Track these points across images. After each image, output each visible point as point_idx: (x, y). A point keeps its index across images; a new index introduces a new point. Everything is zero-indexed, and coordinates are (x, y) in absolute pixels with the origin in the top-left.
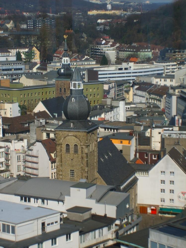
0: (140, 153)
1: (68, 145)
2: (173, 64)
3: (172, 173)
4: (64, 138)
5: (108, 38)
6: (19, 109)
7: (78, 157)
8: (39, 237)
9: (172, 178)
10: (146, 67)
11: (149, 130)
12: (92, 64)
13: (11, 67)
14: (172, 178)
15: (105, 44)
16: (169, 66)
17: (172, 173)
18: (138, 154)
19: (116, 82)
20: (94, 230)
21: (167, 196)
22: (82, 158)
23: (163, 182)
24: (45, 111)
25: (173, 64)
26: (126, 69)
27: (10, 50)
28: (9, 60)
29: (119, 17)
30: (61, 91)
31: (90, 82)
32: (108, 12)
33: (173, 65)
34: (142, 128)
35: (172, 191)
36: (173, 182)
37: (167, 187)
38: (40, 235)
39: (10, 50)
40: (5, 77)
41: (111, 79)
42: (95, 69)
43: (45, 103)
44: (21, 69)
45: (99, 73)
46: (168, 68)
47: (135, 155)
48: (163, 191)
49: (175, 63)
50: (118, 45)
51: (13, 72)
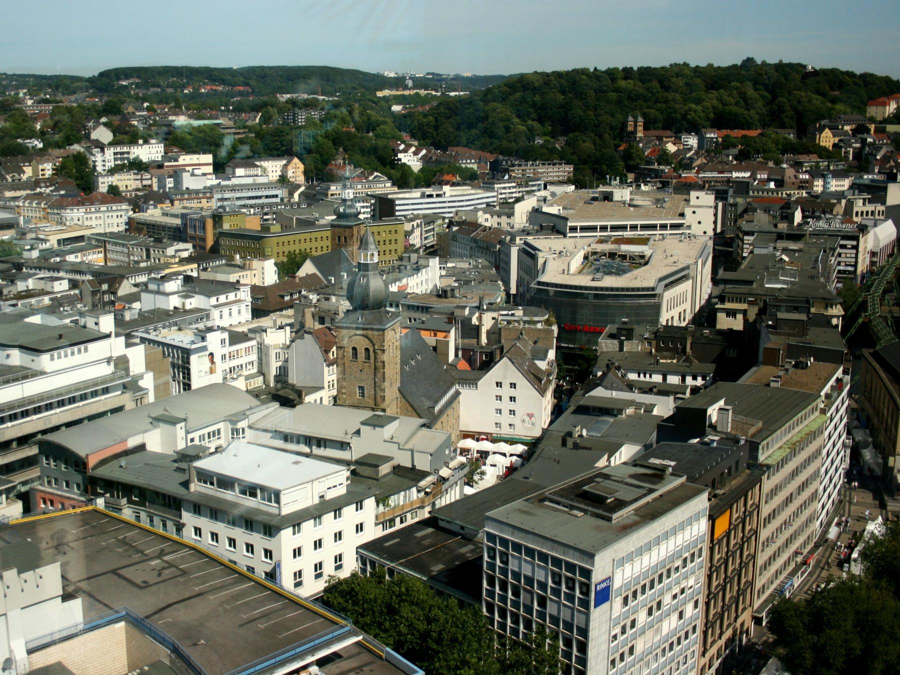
0: (463, 350)
1: (354, 349)
2: (510, 185)
3: (513, 385)
4: (350, 337)
5: (408, 138)
6: (276, 269)
7: (370, 367)
8: (315, 507)
9: (513, 392)
10: (469, 192)
11: (477, 315)
12: (385, 187)
13: (259, 194)
14: (513, 392)
15: (405, 151)
16: (505, 188)
17: (513, 385)
18: (460, 353)
19: (425, 216)
20: (398, 492)
21: (506, 419)
22: (376, 368)
23: (499, 398)
24: (314, 274)
25: (510, 185)
26: (438, 196)
27: (258, 163)
28: (257, 182)
29: (427, 99)
30: (339, 241)
31: (384, 221)
32: (407, 93)
33: (509, 188)
34: (467, 312)
35: (512, 412)
36: (515, 384)
37: (506, 405)
38: (316, 505)
39: (258, 163)
40: (252, 210)
41: (415, 212)
42: (390, 196)
43: (317, 261)
44: (277, 196)
45: (397, 202)
46: (503, 191)
47: (456, 355)
48: (499, 398)
49: (514, 184)
50: (424, 152)
51: (264, 201)
